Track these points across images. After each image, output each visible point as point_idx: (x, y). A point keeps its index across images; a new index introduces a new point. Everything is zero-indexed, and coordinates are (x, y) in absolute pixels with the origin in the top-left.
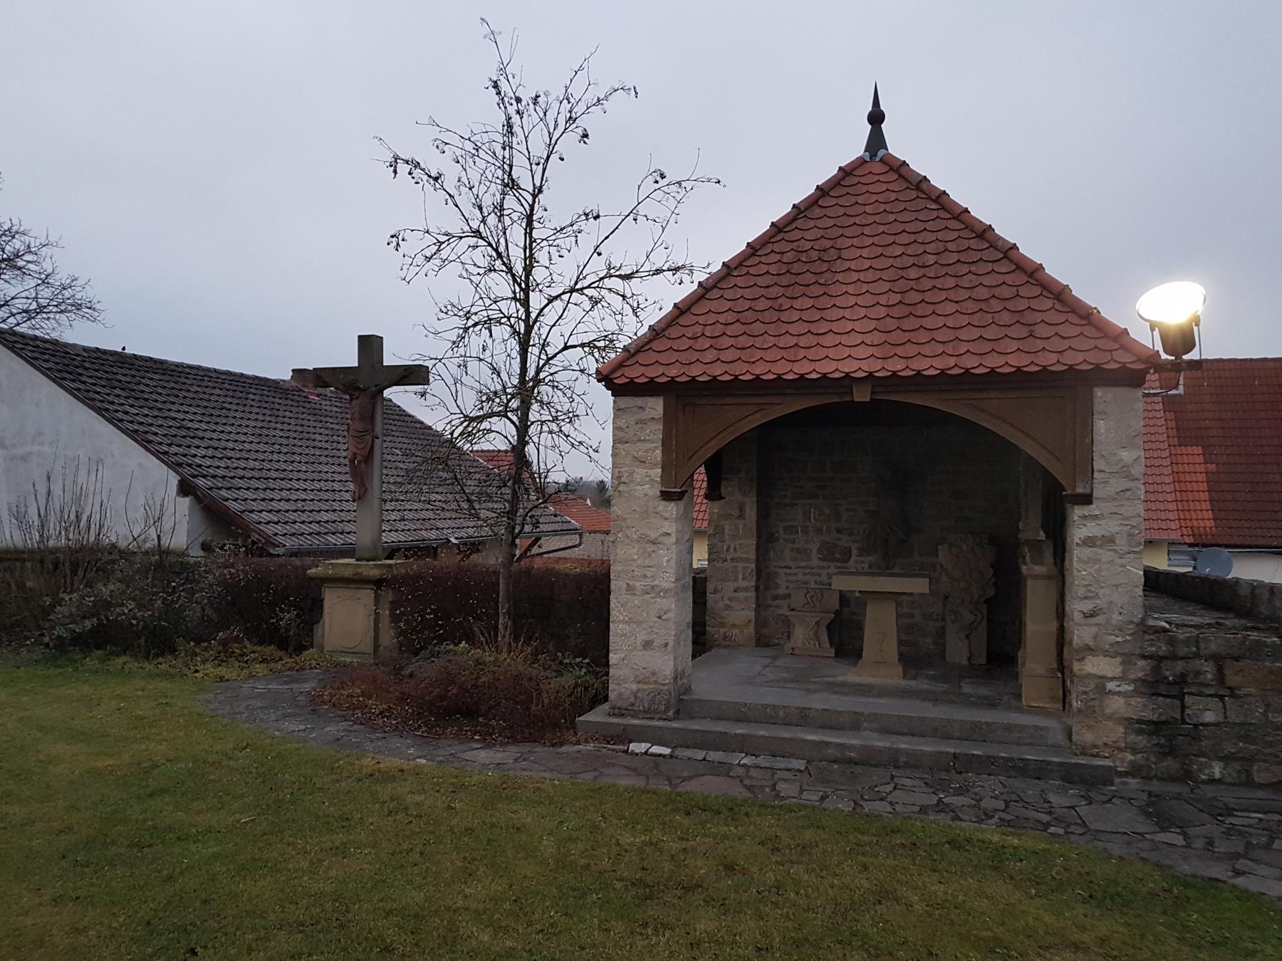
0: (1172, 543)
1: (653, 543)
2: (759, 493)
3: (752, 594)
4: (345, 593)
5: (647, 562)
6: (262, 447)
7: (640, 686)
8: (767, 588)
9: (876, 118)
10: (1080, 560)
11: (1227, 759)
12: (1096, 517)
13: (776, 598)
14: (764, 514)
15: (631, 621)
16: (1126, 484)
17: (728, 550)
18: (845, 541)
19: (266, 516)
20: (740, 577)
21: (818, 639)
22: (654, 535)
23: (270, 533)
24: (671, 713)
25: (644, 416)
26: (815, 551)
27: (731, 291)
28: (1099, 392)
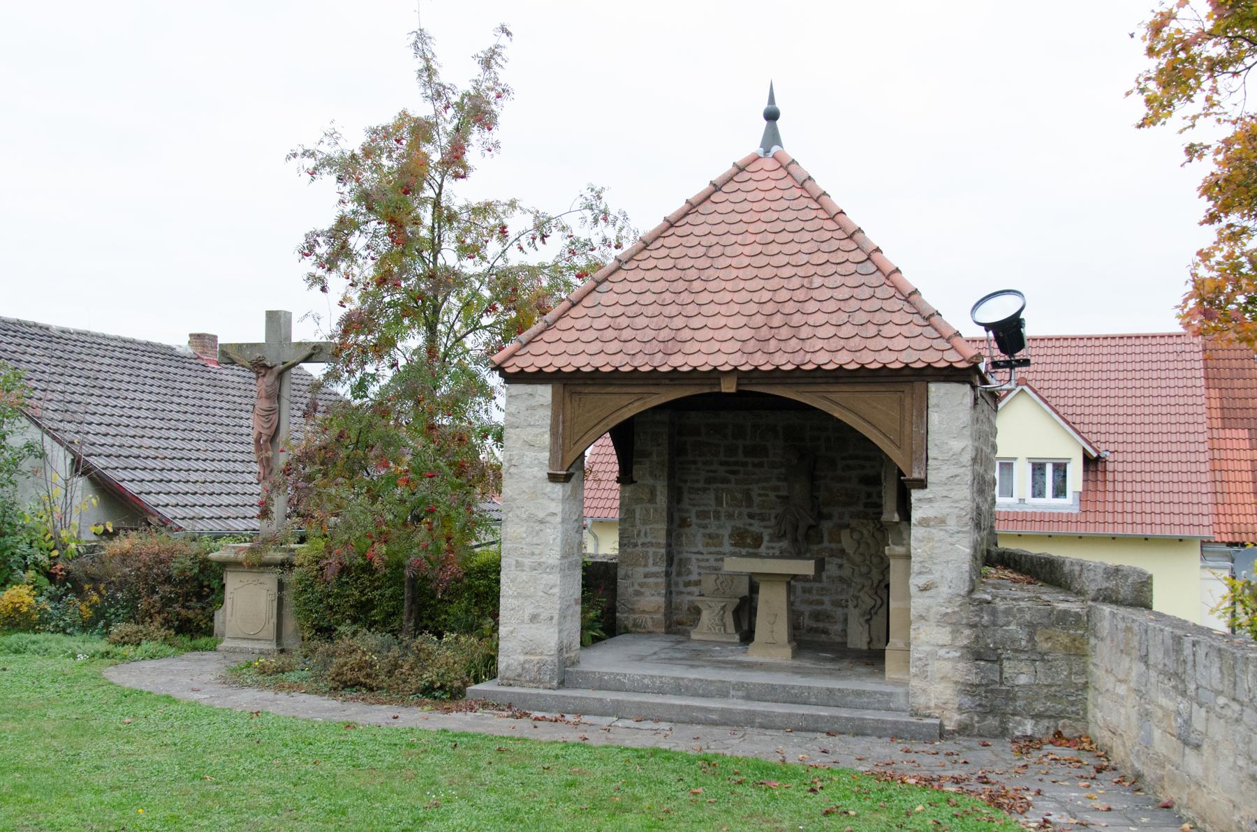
0: (1204, 543)
1: (542, 522)
2: (671, 477)
3: (662, 580)
4: (248, 577)
5: (535, 540)
6: (157, 423)
7: (528, 657)
8: (679, 574)
9: (772, 116)
10: (916, 539)
11: (1037, 717)
12: (930, 500)
13: (687, 584)
14: (675, 495)
15: (519, 595)
16: (954, 470)
17: (638, 535)
18: (756, 527)
19: (164, 499)
20: (651, 561)
21: (724, 626)
22: (541, 515)
23: (169, 516)
24: (555, 683)
25: (533, 402)
26: (726, 537)
27: (620, 285)
28: (933, 387)
